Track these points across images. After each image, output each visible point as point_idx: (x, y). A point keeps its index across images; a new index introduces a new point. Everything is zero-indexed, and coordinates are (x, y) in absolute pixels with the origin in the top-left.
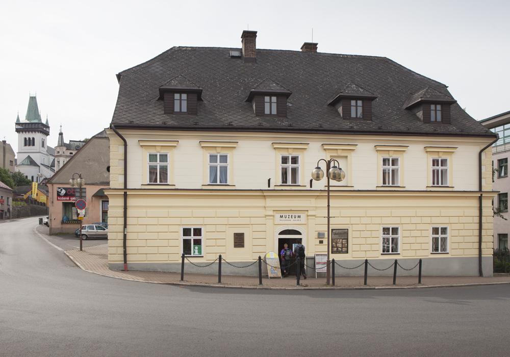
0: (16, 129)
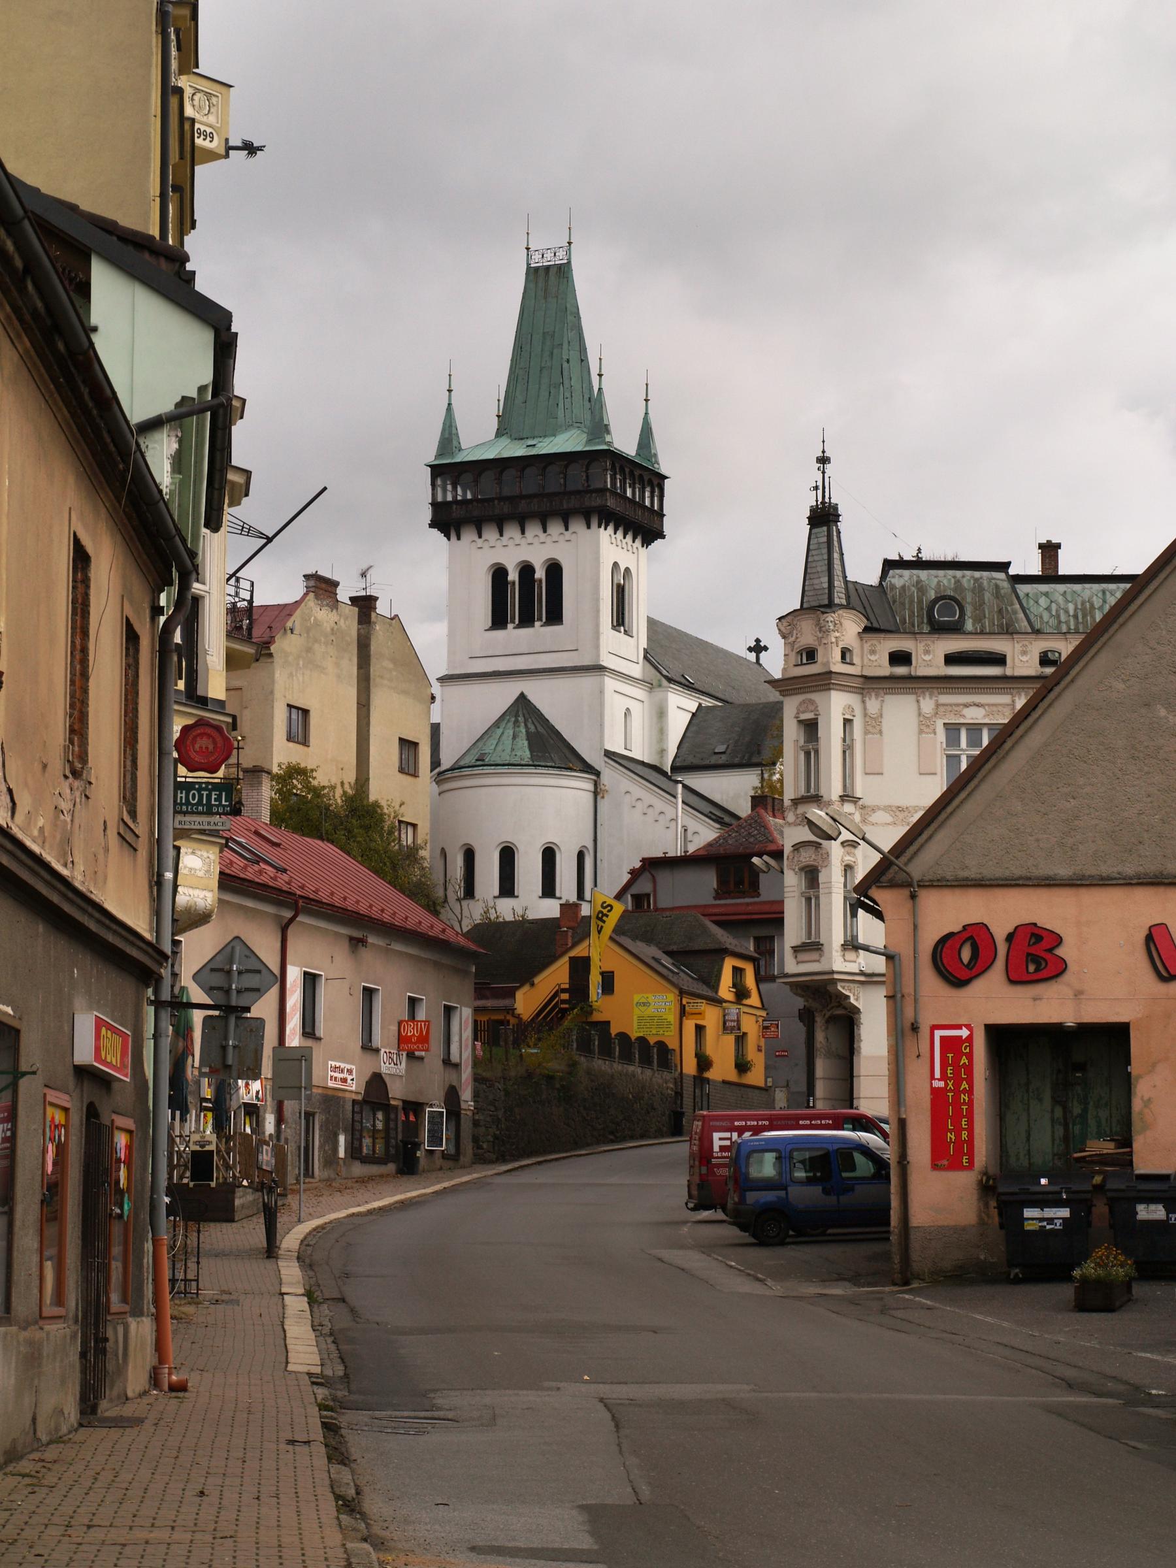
0: (434, 504)
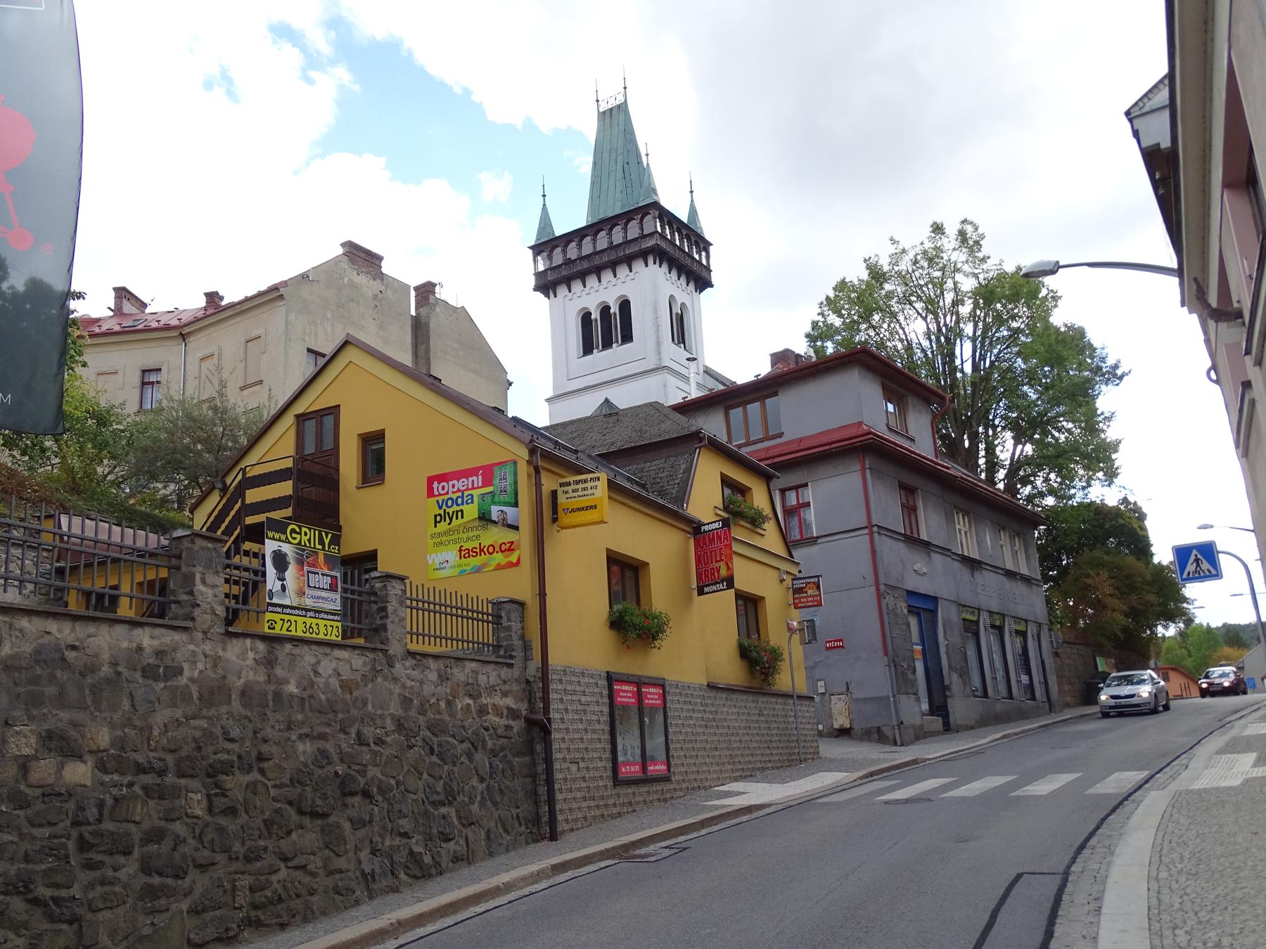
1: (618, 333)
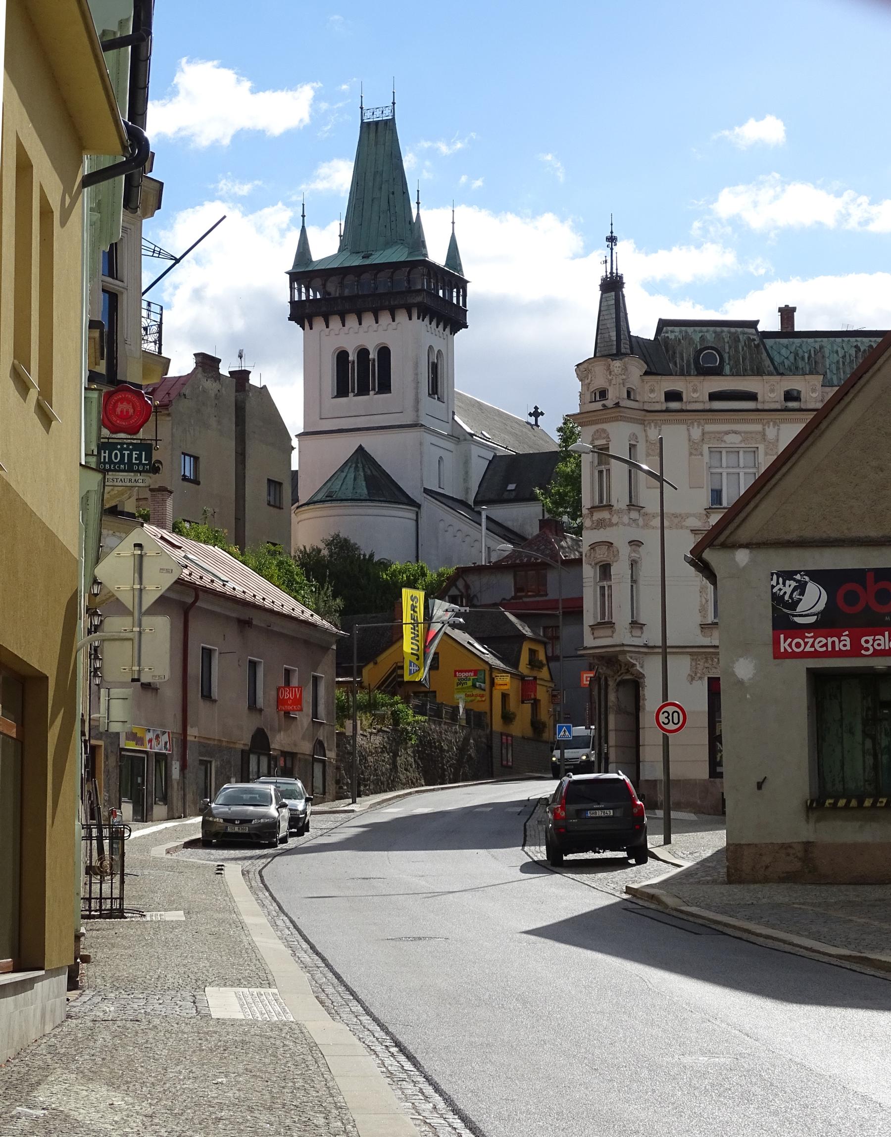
0: (292, 302)
1: (374, 380)
